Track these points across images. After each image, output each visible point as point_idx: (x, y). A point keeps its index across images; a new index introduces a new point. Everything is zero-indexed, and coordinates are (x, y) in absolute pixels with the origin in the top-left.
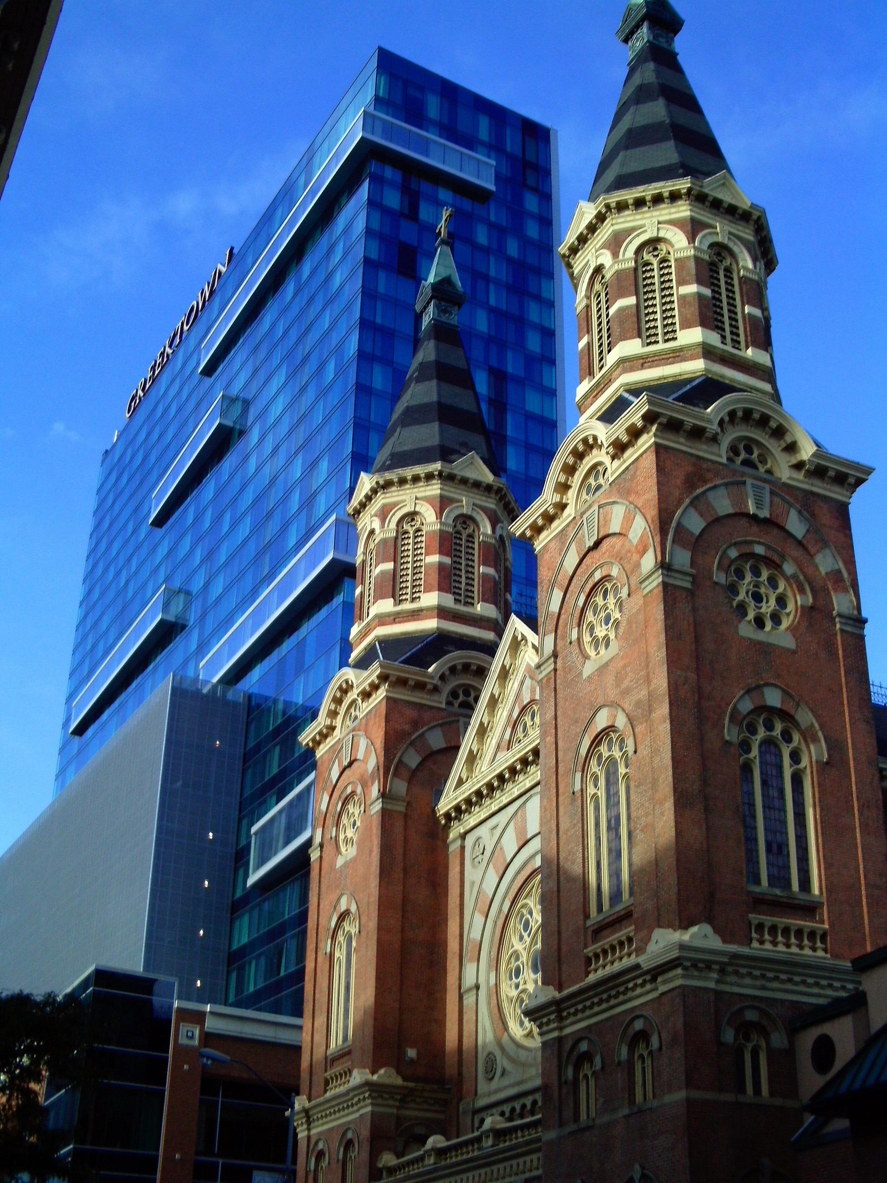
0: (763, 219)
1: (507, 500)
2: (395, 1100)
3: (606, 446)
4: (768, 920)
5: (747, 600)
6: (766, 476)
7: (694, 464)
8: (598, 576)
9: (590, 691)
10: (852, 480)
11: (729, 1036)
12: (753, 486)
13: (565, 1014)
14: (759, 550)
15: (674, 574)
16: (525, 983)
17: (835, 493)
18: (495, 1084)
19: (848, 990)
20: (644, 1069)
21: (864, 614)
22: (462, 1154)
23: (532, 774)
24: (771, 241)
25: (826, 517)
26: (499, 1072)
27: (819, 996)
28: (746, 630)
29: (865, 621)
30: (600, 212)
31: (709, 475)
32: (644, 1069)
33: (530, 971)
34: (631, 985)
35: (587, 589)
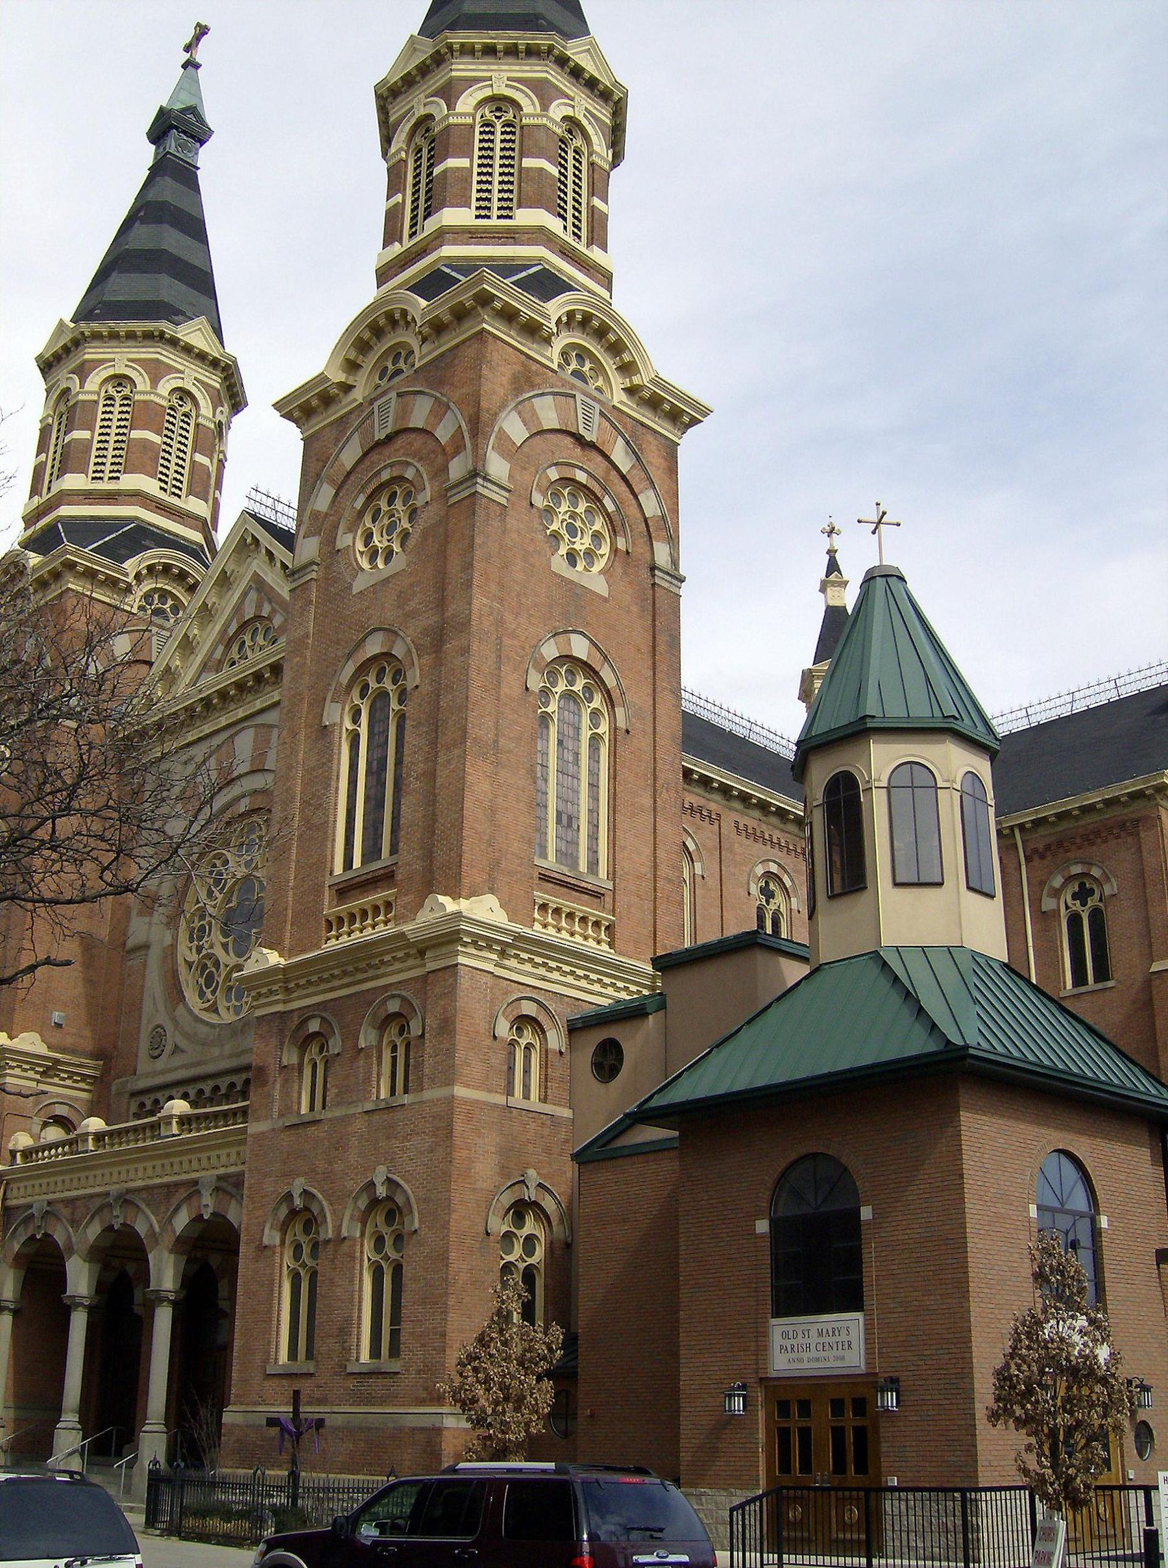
0: (623, 103)
1: (233, 381)
2: (37, 1072)
3: (419, 324)
4: (554, 901)
5: (561, 532)
6: (596, 394)
7: (523, 364)
8: (385, 476)
9: (361, 609)
10: (686, 419)
11: (503, 1029)
12: (583, 403)
13: (292, 985)
14: (581, 477)
15: (489, 485)
16: (211, 947)
17: (664, 429)
18: (160, 1064)
19: (631, 993)
20: (394, 1059)
21: (683, 571)
22: (128, 1142)
23: (249, 703)
24: (624, 131)
25: (654, 459)
26: (169, 1048)
27: (600, 994)
28: (559, 563)
29: (682, 580)
30: (438, 52)
31: (537, 380)
32: (394, 1059)
33: (219, 933)
34: (387, 958)
35: (372, 487)
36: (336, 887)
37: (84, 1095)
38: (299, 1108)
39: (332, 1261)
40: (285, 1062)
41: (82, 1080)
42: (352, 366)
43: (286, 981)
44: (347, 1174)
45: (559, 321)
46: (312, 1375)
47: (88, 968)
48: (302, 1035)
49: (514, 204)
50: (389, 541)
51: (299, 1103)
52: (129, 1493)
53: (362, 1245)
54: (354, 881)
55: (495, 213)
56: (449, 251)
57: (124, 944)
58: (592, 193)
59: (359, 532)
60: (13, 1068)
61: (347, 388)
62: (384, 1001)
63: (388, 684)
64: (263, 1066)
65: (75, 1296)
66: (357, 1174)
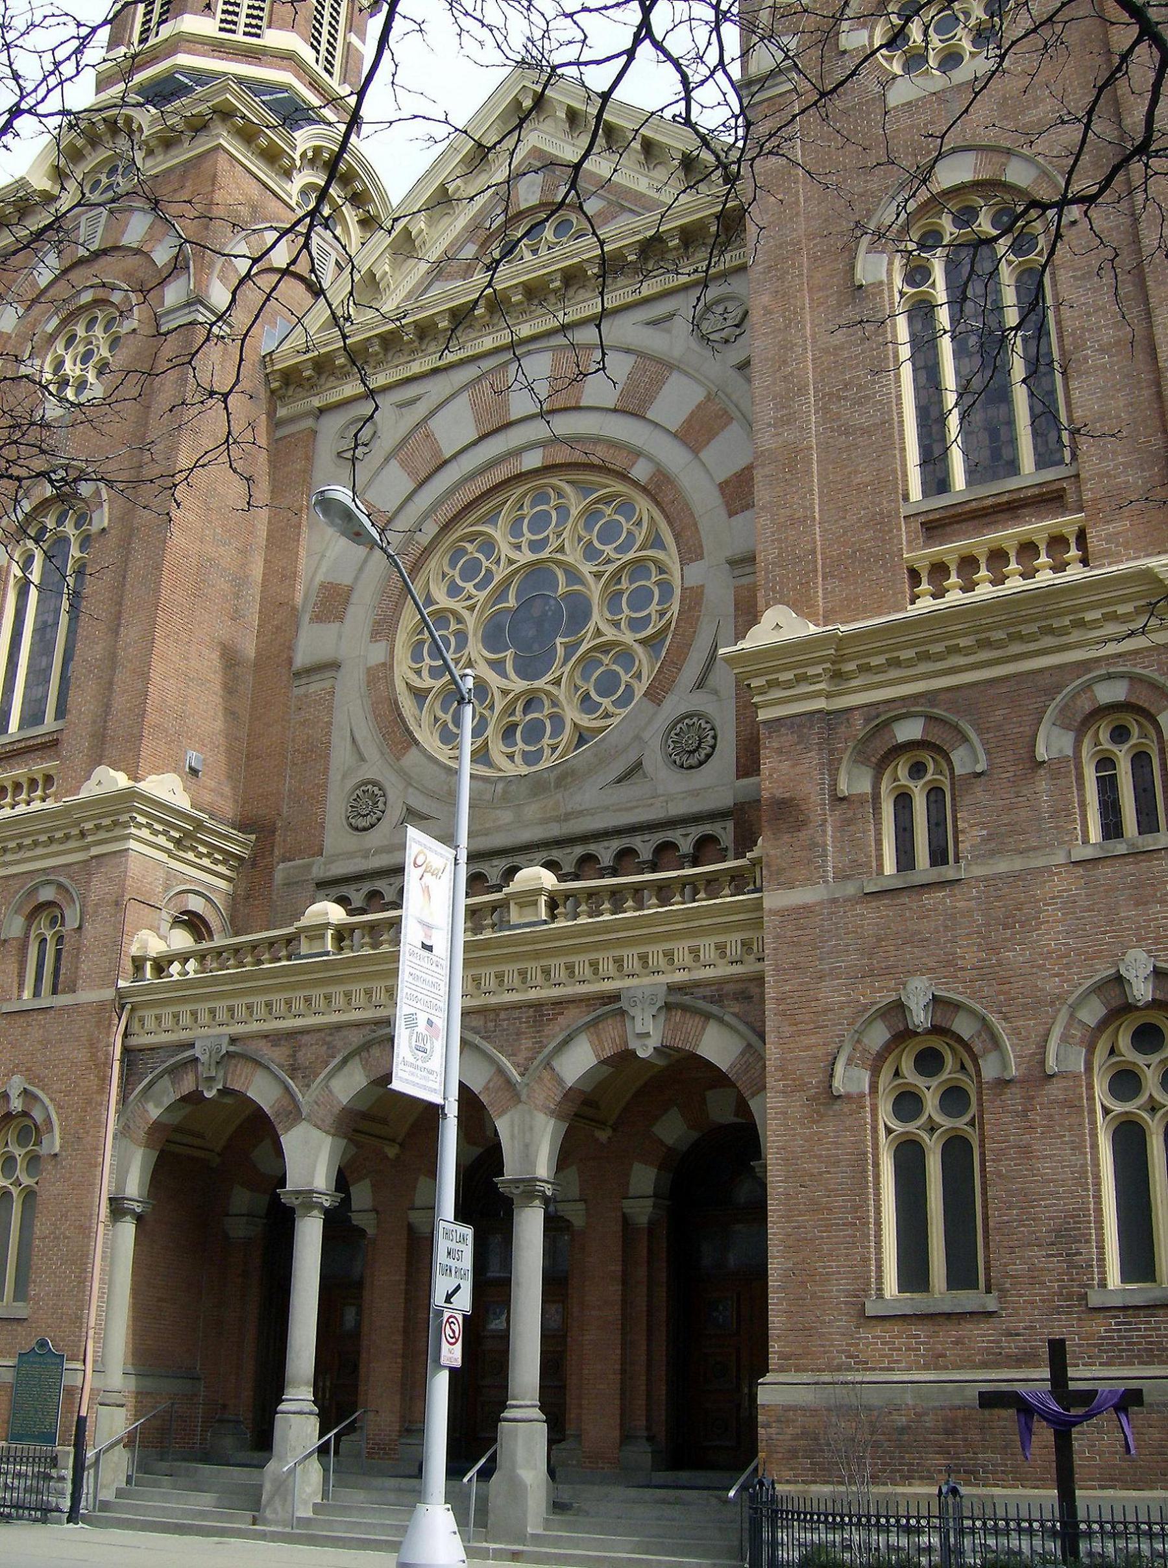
8: (86, 297)
36: (922, 519)
37: (222, 884)
38: (880, 866)
39: (1024, 1114)
40: (843, 788)
41: (224, 862)
42: (59, 175)
43: (840, 659)
44: (1040, 967)
45: (303, 155)
46: (991, 1314)
47: (230, 693)
48: (880, 746)
49: (264, 24)
50: (82, 370)
51: (880, 857)
52: (485, 1527)
53: (1090, 1087)
54: (967, 508)
55: (241, 28)
56: (184, 59)
57: (290, 661)
58: (350, 28)
59: (49, 359)
60: (139, 826)
61: (49, 198)
62: (1088, 687)
63: (69, 529)
64: (792, 799)
65: (312, 1191)
66: (1068, 966)
